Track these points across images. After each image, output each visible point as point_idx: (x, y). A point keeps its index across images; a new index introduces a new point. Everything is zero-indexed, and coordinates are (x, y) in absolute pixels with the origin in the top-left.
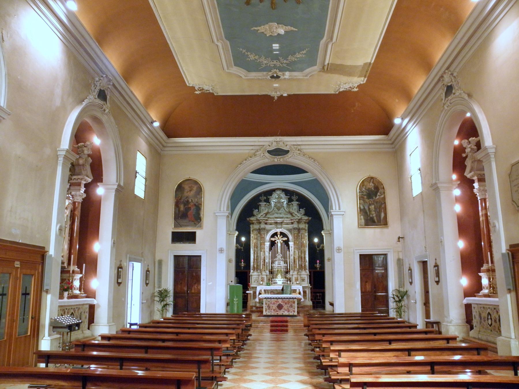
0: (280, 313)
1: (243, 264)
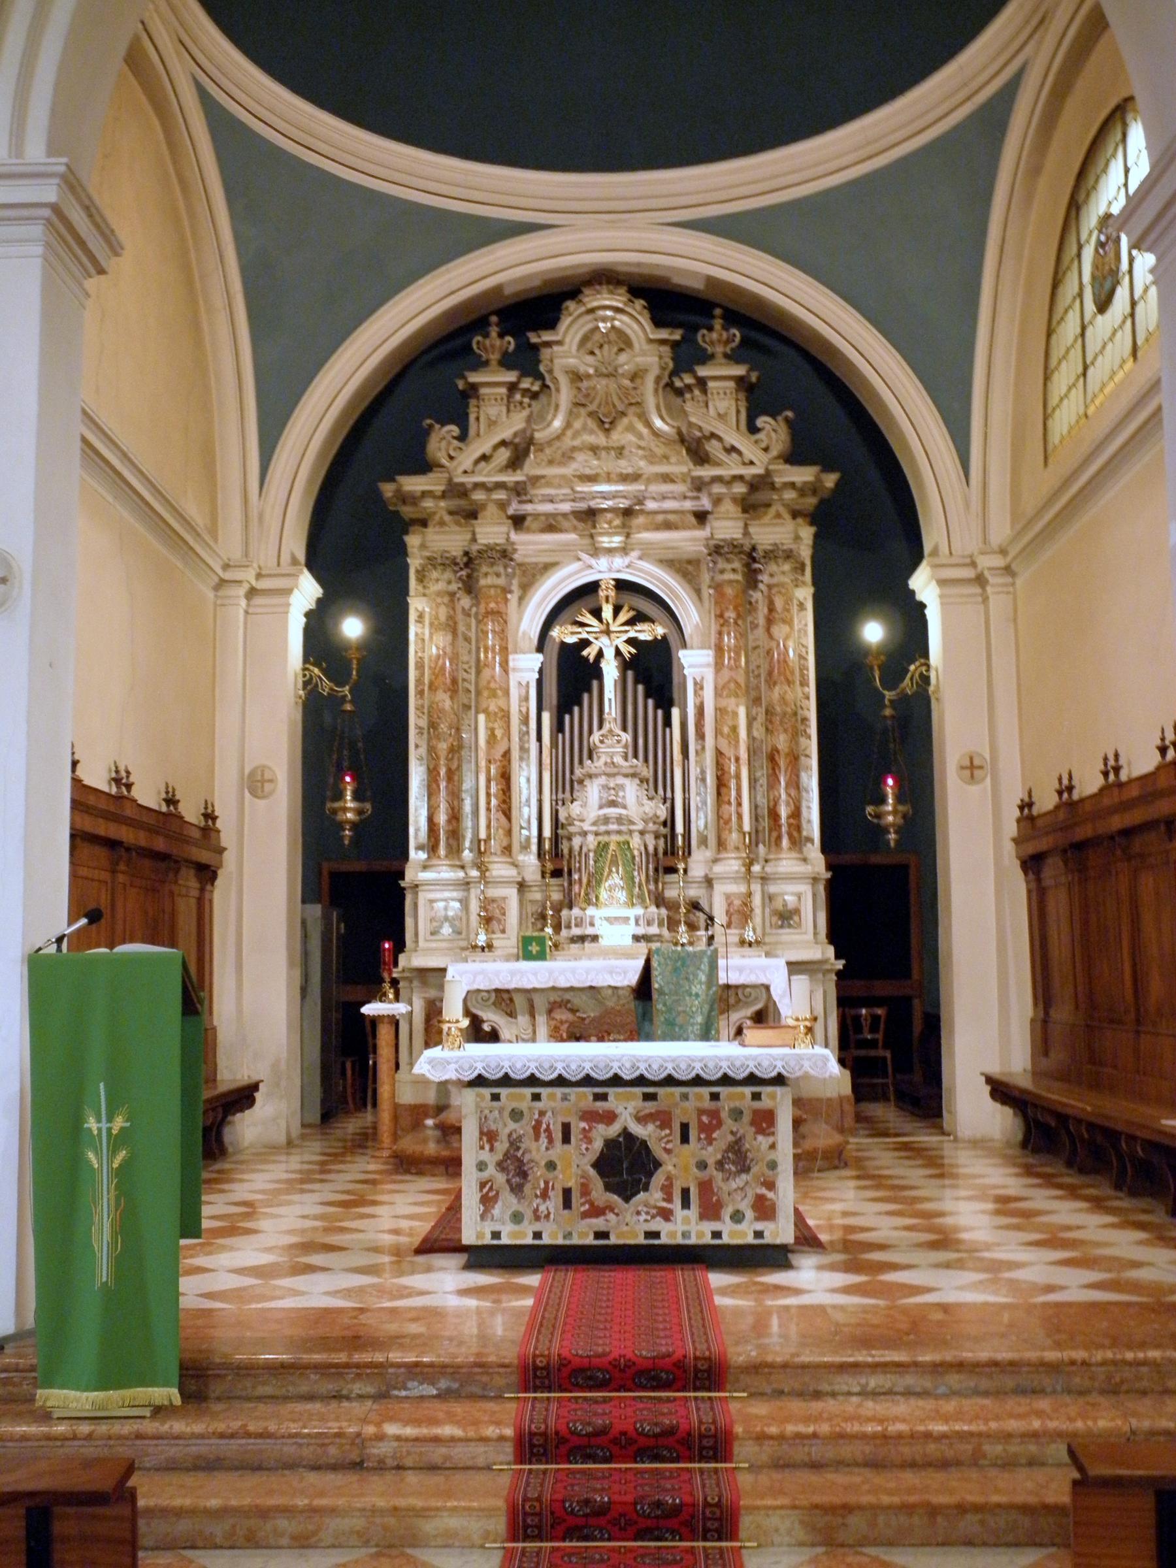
0: (630, 1224)
1: (349, 807)
